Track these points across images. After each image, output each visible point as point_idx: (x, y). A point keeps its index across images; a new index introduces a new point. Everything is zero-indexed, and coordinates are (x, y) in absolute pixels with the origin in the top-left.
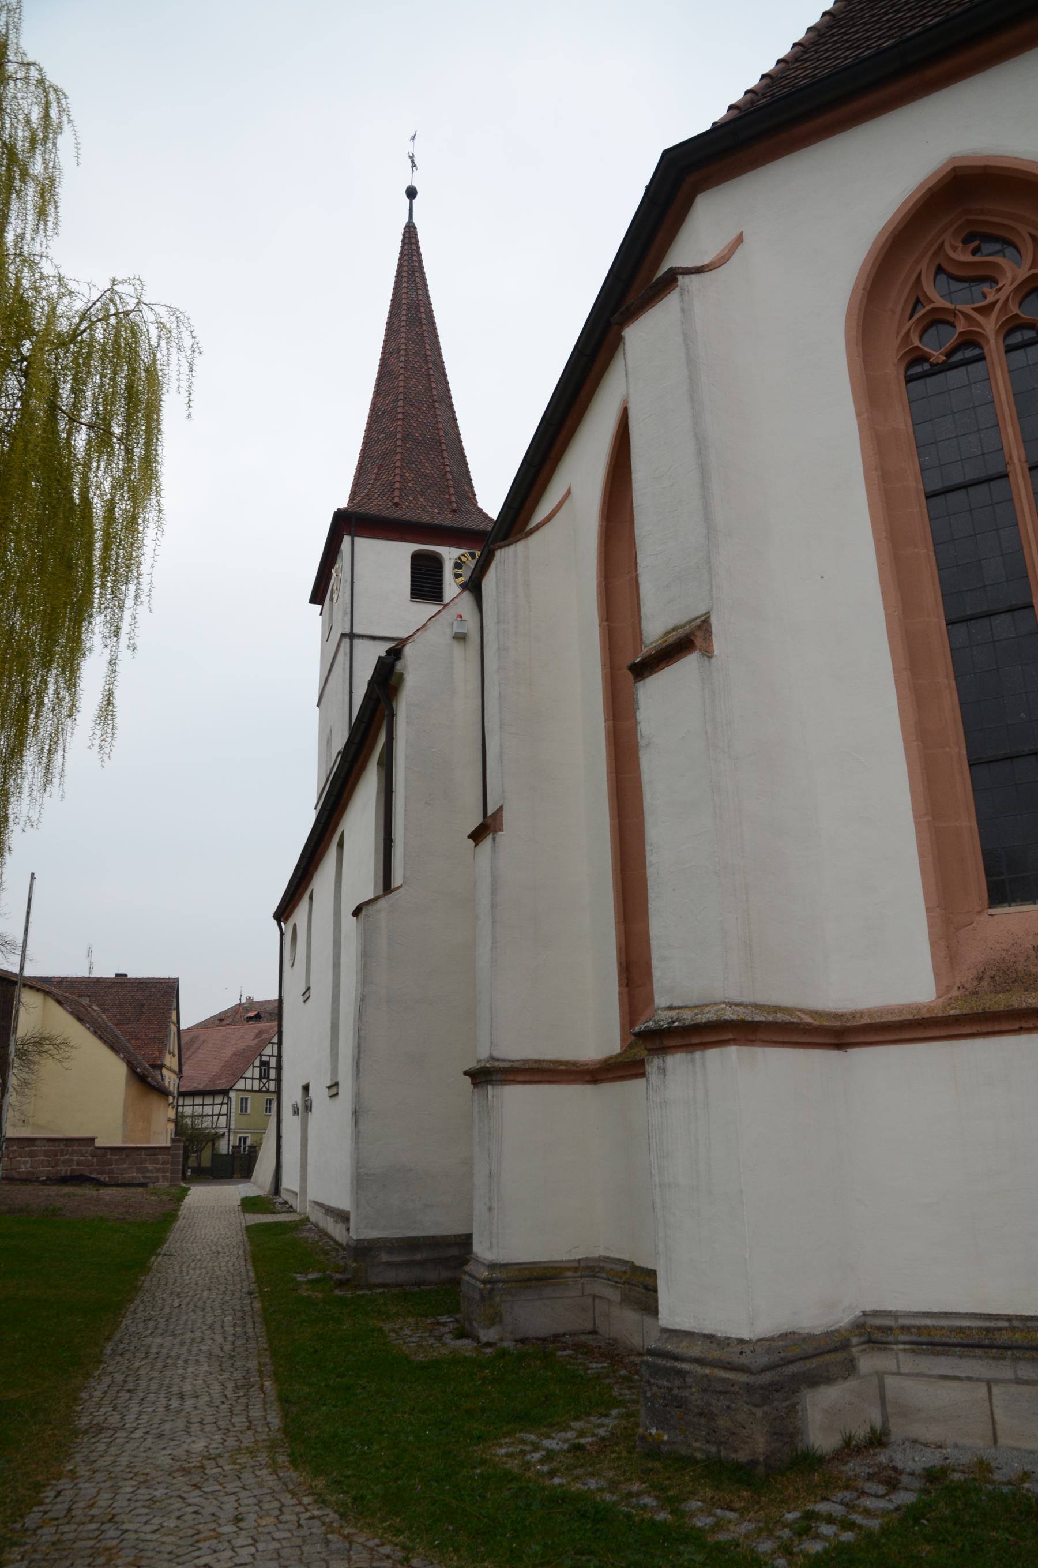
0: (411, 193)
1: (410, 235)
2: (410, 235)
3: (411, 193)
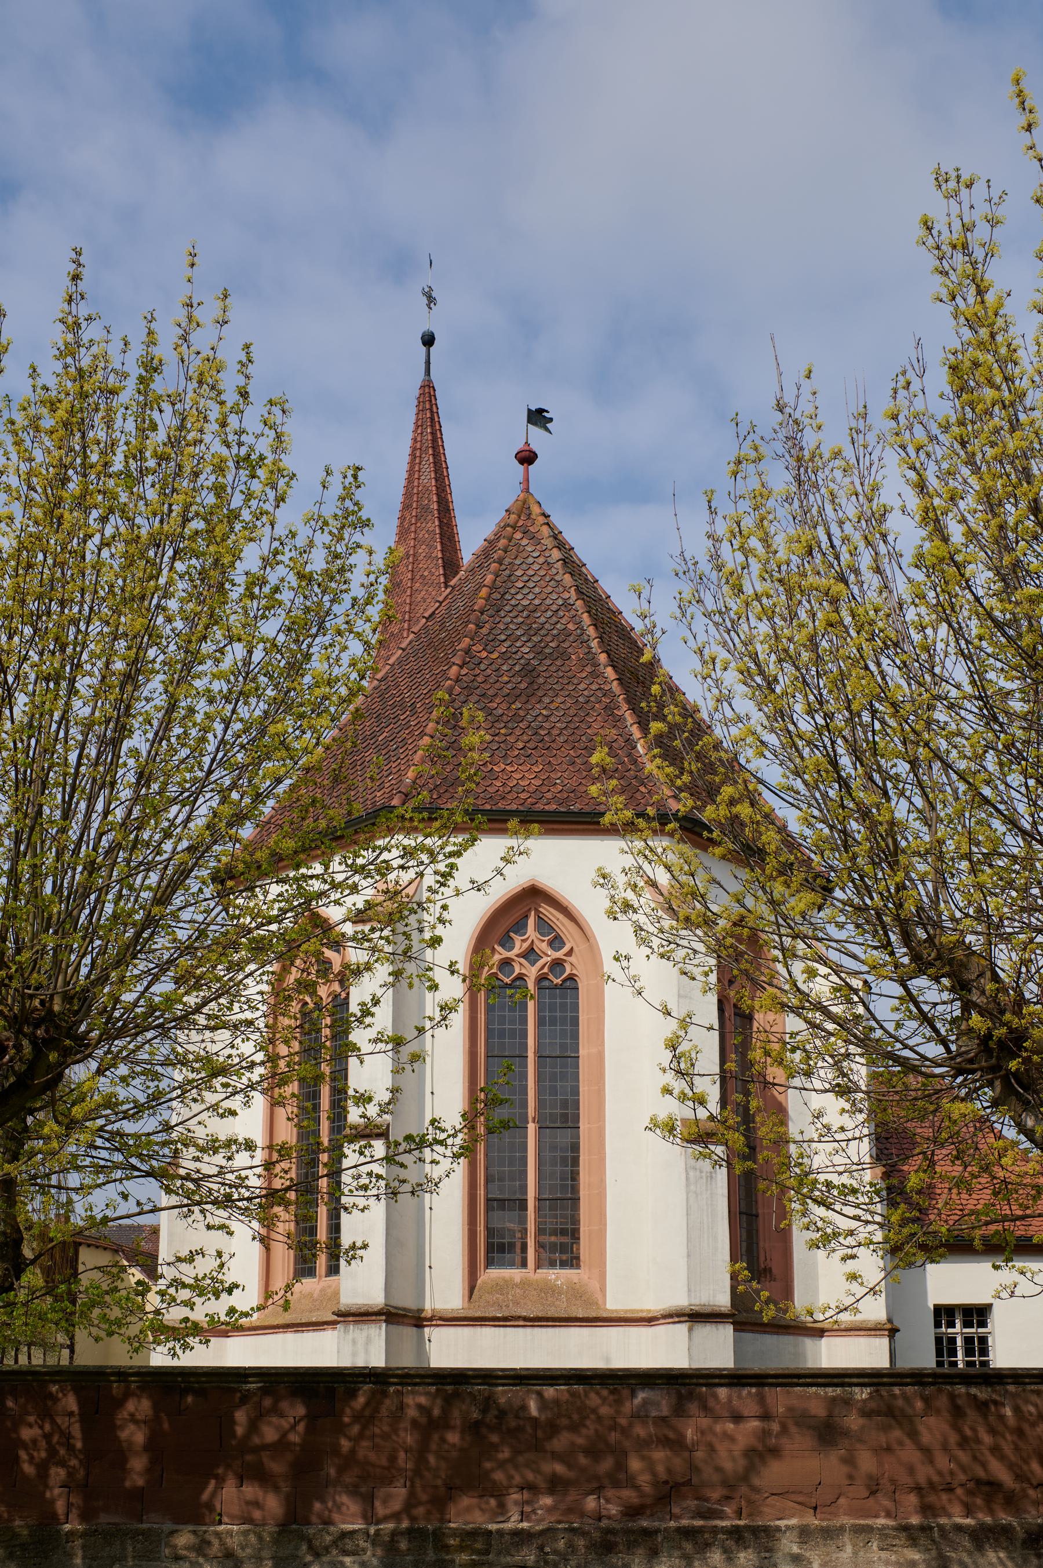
0: (428, 340)
1: (428, 395)
2: (428, 395)
3: (428, 340)
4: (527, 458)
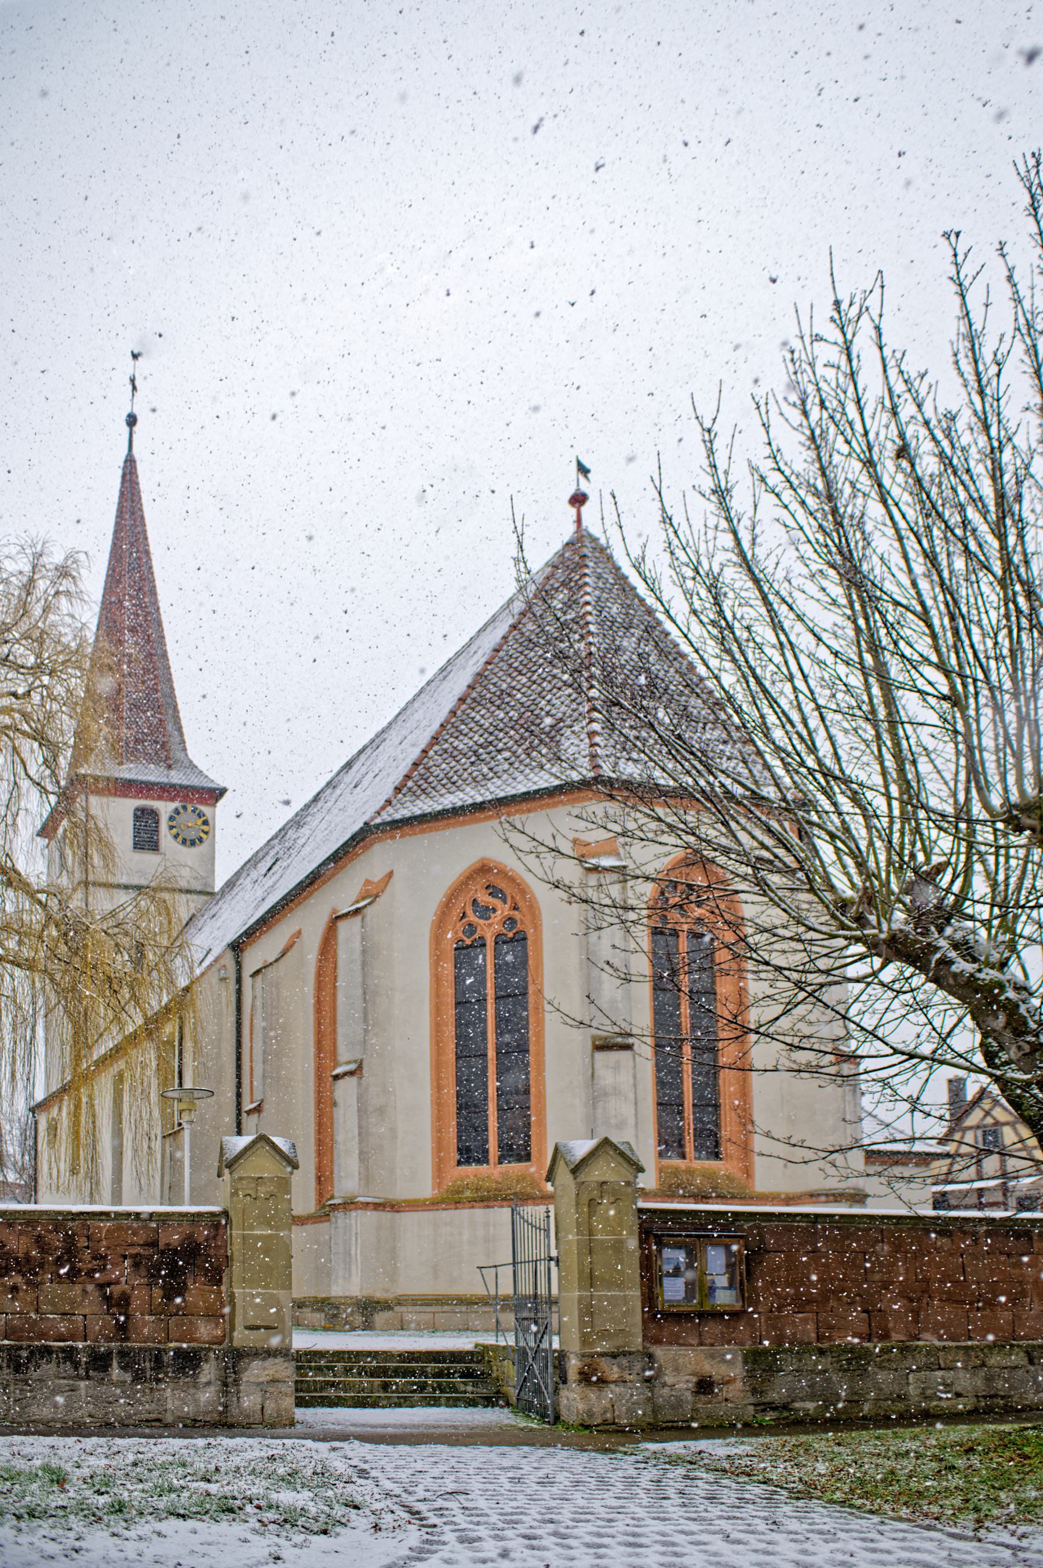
1: (130, 463)
2: (130, 463)
3: (132, 421)
4: (578, 500)
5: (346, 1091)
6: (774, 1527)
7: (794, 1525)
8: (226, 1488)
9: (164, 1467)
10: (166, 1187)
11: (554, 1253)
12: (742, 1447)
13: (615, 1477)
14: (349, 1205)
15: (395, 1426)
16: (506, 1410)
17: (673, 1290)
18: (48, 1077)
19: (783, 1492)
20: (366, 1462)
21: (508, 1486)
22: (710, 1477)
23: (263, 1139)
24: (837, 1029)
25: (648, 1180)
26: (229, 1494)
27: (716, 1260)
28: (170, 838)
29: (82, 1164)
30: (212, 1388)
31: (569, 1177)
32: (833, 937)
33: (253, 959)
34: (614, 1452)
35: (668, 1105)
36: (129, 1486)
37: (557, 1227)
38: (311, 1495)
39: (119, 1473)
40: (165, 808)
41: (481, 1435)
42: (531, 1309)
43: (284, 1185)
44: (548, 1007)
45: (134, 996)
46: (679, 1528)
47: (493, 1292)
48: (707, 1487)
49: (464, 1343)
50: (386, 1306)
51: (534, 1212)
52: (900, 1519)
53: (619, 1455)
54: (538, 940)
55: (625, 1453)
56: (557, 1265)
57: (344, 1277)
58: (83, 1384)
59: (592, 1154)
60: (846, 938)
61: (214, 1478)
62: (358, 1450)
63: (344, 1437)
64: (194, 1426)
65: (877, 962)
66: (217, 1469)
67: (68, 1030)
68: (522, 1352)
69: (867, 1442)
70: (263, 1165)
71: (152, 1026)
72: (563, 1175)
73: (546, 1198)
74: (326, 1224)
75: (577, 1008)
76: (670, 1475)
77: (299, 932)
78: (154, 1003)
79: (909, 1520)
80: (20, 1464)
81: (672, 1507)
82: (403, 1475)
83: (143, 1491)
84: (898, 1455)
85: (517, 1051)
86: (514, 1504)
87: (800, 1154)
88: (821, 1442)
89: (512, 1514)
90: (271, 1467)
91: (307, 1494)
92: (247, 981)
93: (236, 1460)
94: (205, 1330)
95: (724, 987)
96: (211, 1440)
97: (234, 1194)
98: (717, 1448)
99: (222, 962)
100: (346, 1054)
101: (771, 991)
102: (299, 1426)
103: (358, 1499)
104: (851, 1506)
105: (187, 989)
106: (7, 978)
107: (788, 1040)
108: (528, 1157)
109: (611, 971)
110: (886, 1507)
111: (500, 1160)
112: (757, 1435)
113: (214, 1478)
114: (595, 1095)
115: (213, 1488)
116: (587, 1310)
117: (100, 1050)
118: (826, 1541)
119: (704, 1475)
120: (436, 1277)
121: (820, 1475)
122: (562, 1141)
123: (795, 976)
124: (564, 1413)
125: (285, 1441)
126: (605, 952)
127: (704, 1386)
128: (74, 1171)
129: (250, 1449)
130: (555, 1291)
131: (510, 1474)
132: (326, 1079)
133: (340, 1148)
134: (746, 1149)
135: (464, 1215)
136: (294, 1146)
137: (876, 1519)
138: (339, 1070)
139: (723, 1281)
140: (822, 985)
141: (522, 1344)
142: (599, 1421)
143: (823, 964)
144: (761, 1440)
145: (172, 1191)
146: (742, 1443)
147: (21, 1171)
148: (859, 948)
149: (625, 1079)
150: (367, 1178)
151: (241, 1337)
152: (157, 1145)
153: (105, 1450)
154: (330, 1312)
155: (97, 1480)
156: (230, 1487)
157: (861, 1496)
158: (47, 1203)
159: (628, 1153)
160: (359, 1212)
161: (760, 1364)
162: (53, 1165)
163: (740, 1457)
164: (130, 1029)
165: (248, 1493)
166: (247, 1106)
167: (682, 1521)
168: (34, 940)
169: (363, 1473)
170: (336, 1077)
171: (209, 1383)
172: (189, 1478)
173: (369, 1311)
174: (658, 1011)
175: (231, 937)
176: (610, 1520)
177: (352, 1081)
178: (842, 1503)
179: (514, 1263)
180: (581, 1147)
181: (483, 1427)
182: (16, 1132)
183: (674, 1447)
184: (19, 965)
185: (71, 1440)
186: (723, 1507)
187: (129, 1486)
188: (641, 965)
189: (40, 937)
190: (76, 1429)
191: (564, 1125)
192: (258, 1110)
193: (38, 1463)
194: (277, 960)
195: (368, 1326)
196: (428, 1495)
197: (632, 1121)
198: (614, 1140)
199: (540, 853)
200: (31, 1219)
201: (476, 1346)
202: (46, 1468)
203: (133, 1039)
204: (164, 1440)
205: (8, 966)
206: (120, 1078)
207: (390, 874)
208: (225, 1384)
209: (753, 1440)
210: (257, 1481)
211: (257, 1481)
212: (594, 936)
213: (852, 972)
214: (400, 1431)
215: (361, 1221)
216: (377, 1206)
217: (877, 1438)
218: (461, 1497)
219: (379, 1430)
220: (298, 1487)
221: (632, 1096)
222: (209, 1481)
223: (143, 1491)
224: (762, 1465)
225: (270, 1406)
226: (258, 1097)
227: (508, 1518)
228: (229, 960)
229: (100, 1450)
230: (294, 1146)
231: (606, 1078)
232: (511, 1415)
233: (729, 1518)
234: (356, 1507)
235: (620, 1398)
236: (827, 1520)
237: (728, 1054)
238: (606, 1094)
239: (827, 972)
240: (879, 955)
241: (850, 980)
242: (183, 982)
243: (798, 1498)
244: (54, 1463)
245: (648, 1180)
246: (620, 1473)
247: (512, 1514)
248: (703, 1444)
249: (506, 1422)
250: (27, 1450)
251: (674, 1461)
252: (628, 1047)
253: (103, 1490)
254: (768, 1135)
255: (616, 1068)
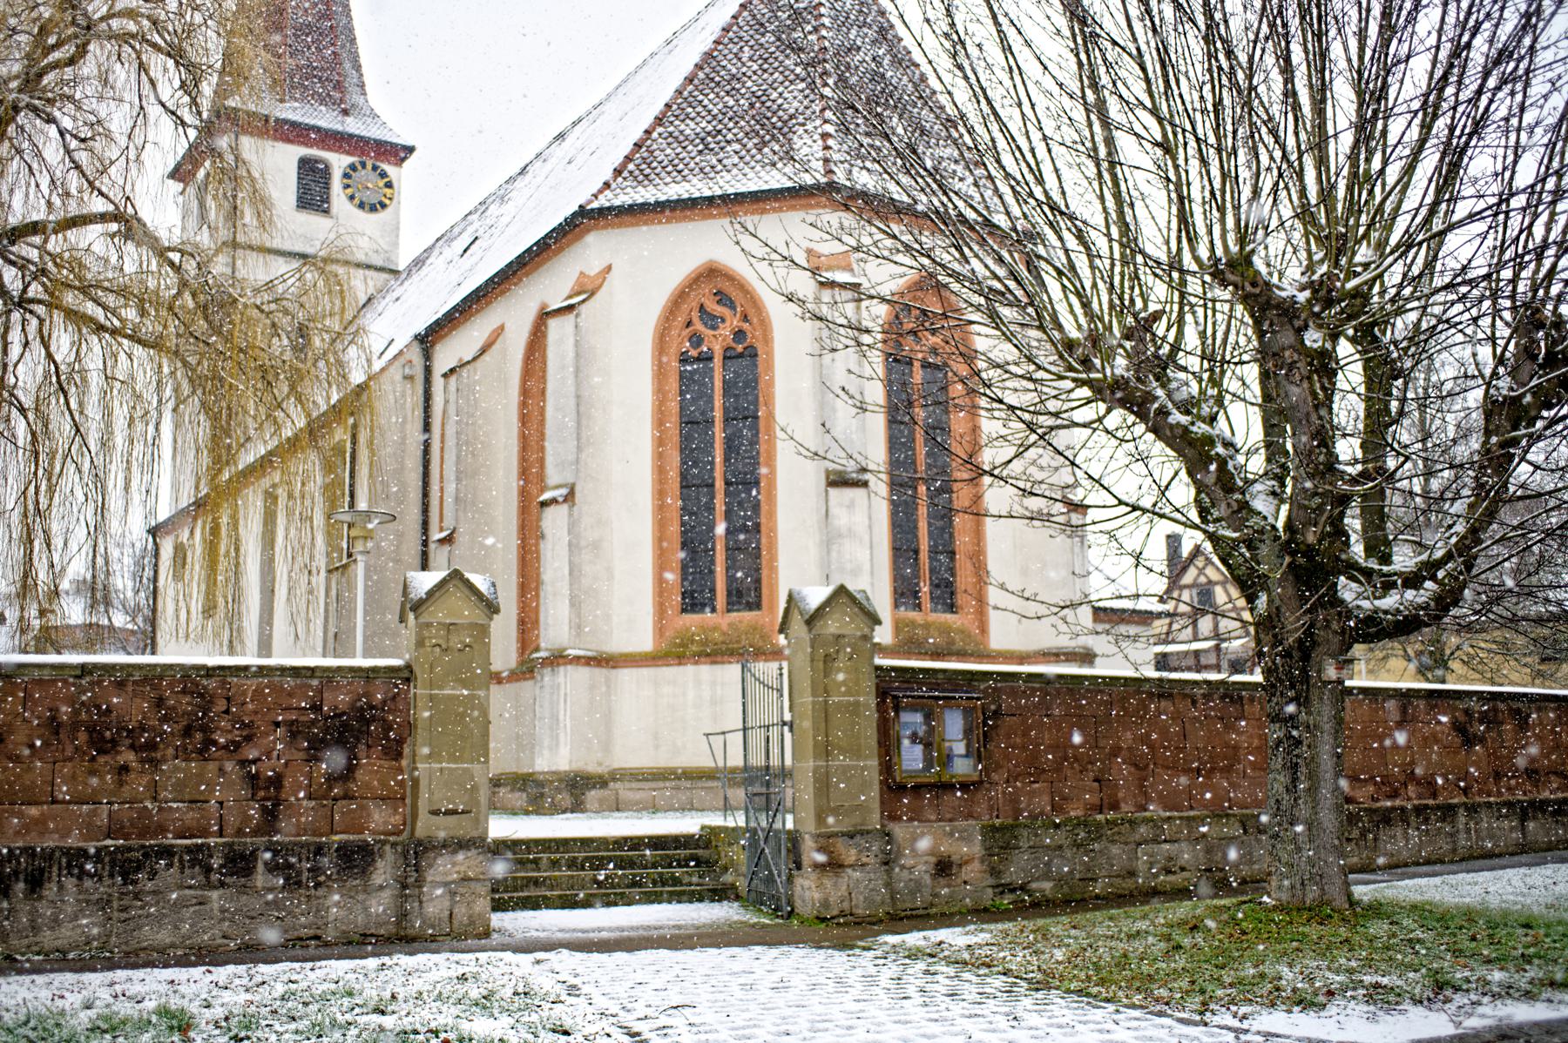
5: (554, 522)
6: (1015, 1023)
7: (1033, 1019)
8: (406, 1020)
9: (324, 998)
10: (331, 635)
11: (787, 717)
12: (982, 935)
13: (854, 976)
14: (558, 659)
15: (610, 930)
16: (736, 904)
17: (912, 758)
18: (176, 487)
19: (1023, 983)
20: (576, 976)
21: (739, 994)
22: (951, 971)
23: (456, 575)
24: (1065, 476)
25: (884, 635)
26: (409, 1028)
27: (954, 725)
28: (344, 198)
29: (219, 605)
30: (386, 894)
31: (805, 628)
32: (1061, 378)
33: (445, 357)
34: (852, 947)
35: (903, 550)
36: (277, 1027)
37: (790, 681)
38: (512, 1021)
39: (264, 1011)
40: (339, 162)
41: (709, 936)
42: (761, 784)
43: (483, 631)
44: (780, 434)
45: (292, 388)
46: (922, 1031)
47: (721, 764)
48: (947, 982)
49: (689, 824)
50: (601, 782)
51: (767, 669)
52: (1133, 1006)
53: (857, 951)
54: (770, 354)
55: (864, 949)
56: (791, 730)
57: (551, 749)
58: (215, 894)
59: (828, 602)
60: (1074, 380)
61: (390, 1009)
62: (565, 961)
63: (550, 946)
64: (356, 943)
65: (1102, 407)
66: (393, 997)
67: (204, 429)
68: (754, 832)
69: (1102, 923)
70: (463, 611)
71: (314, 430)
72: (797, 626)
73: (777, 654)
74: (530, 683)
75: (808, 434)
76: (910, 971)
77: (502, 328)
78: (321, 401)
79: (1142, 1007)
80: (125, 1009)
81: (913, 1008)
82: (621, 990)
83: (297, 1032)
84: (1130, 937)
85: (747, 481)
86: (747, 1015)
87: (1033, 608)
88: (1057, 926)
89: (743, 1028)
90: (462, 989)
91: (506, 1021)
92: (438, 383)
93: (418, 984)
94: (380, 817)
95: (958, 422)
96: (386, 959)
97: (420, 643)
98: (955, 937)
99: (407, 356)
100: (555, 474)
101: (1004, 432)
102: (495, 936)
103: (568, 1023)
104: (1088, 995)
105: (362, 388)
106: (122, 357)
107: (1021, 484)
108: (756, 605)
109: (846, 397)
110: (1120, 993)
111: (731, 606)
112: (996, 921)
113: (390, 1009)
114: (830, 537)
115: (388, 1021)
116: (823, 784)
117: (247, 458)
118: (1065, 1035)
119: (945, 969)
120: (657, 747)
121: (1058, 962)
122: (796, 588)
123: (1027, 416)
124: (798, 903)
125: (478, 955)
126: (839, 377)
127: (944, 867)
128: (209, 610)
129: (432, 969)
130: (788, 762)
131: (742, 981)
132: (531, 509)
133: (547, 590)
134: (981, 600)
135: (689, 671)
136: (494, 585)
137: (1111, 1007)
138: (546, 496)
139: (960, 748)
140: (1052, 428)
141: (753, 824)
142: (835, 913)
143: (1052, 405)
144: (1000, 926)
145: (338, 641)
146: (982, 930)
147: (133, 613)
148: (1085, 392)
149: (859, 519)
150: (577, 627)
151: (426, 826)
152: (320, 580)
153: (245, 981)
154: (536, 792)
155: (234, 1021)
156: (410, 1019)
157: (1100, 983)
158: (172, 653)
159: (865, 602)
160: (569, 667)
161: (1001, 840)
162: (182, 604)
163: (980, 946)
164: (288, 432)
165: (433, 1025)
166: (436, 535)
167: (924, 1023)
168: (164, 313)
169: (573, 990)
170: (544, 504)
171: (381, 888)
172: (357, 1010)
173: (577, 789)
174: (893, 444)
175: (420, 326)
176: (850, 1028)
177: (563, 509)
178: (1079, 992)
179: (745, 729)
180: (815, 596)
181: (711, 926)
182: (127, 560)
183: (914, 939)
184: (139, 342)
185: (197, 972)
186: (965, 1004)
187: (277, 1027)
188: (876, 393)
189: (170, 308)
190: (208, 956)
191: (799, 570)
192: (448, 540)
193: (150, 1005)
194: (475, 359)
195: (577, 807)
196: (649, 1012)
197: (867, 566)
198: (851, 587)
199: (774, 258)
200: (153, 677)
201: (703, 828)
202: (164, 1012)
203: (293, 444)
204: (323, 963)
205: (125, 342)
206: (271, 497)
207: (609, 268)
208: (404, 887)
209: (992, 927)
210: (444, 1009)
211: (444, 1009)
212: (828, 357)
213: (1078, 416)
214: (612, 935)
215: (571, 680)
216: (588, 661)
217: (1111, 919)
218: (687, 1011)
219: (591, 935)
220: (496, 1012)
221: (867, 538)
222: (383, 1013)
223: (297, 1032)
224: (1002, 955)
225: (461, 912)
226: (449, 522)
227: (741, 1032)
228: (416, 355)
229: (237, 981)
230: (494, 585)
231: (841, 517)
232: (742, 911)
233: (970, 1016)
234: (566, 1033)
235: (859, 885)
236: (1065, 1011)
237: (962, 497)
238: (840, 535)
239: (1056, 415)
240: (1104, 401)
241: (1077, 425)
242: (357, 377)
243: (1037, 990)
244: (174, 1003)
245: (884, 635)
246: (859, 972)
247: (743, 1028)
248: (943, 934)
249: (736, 918)
250: (135, 989)
251: (914, 954)
252: (865, 484)
253: (242, 1034)
254: (1002, 587)
255: (851, 506)
